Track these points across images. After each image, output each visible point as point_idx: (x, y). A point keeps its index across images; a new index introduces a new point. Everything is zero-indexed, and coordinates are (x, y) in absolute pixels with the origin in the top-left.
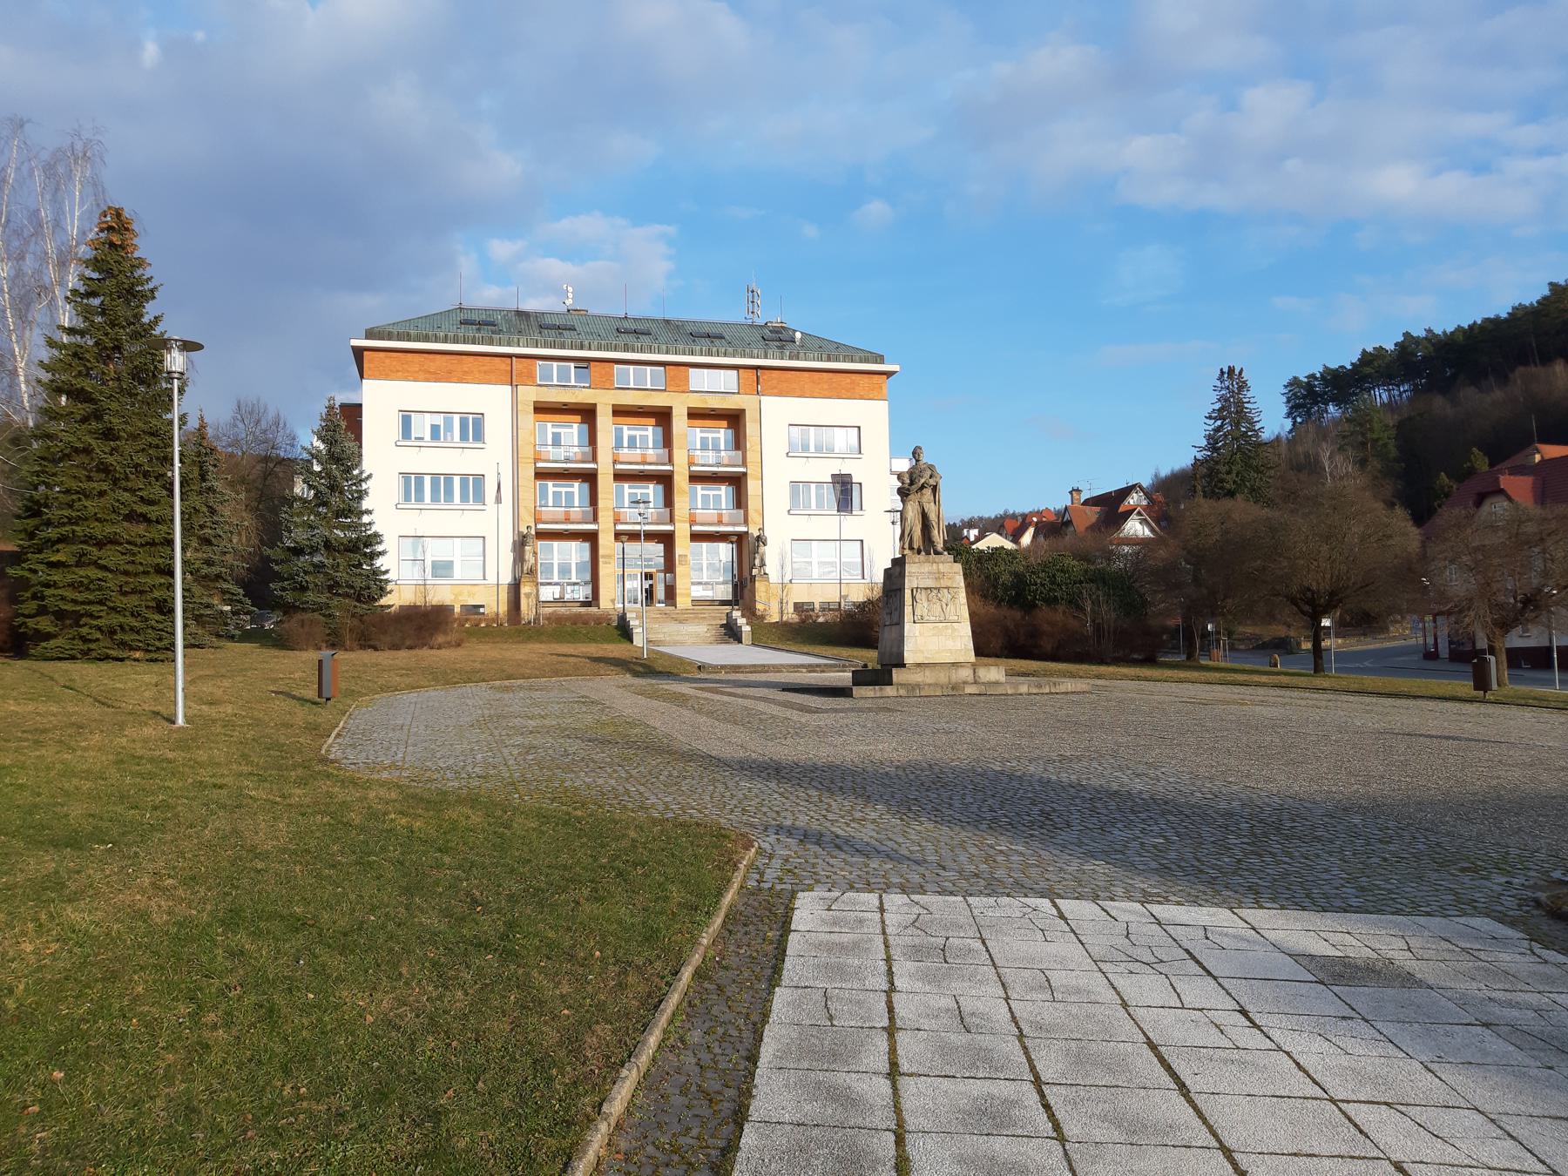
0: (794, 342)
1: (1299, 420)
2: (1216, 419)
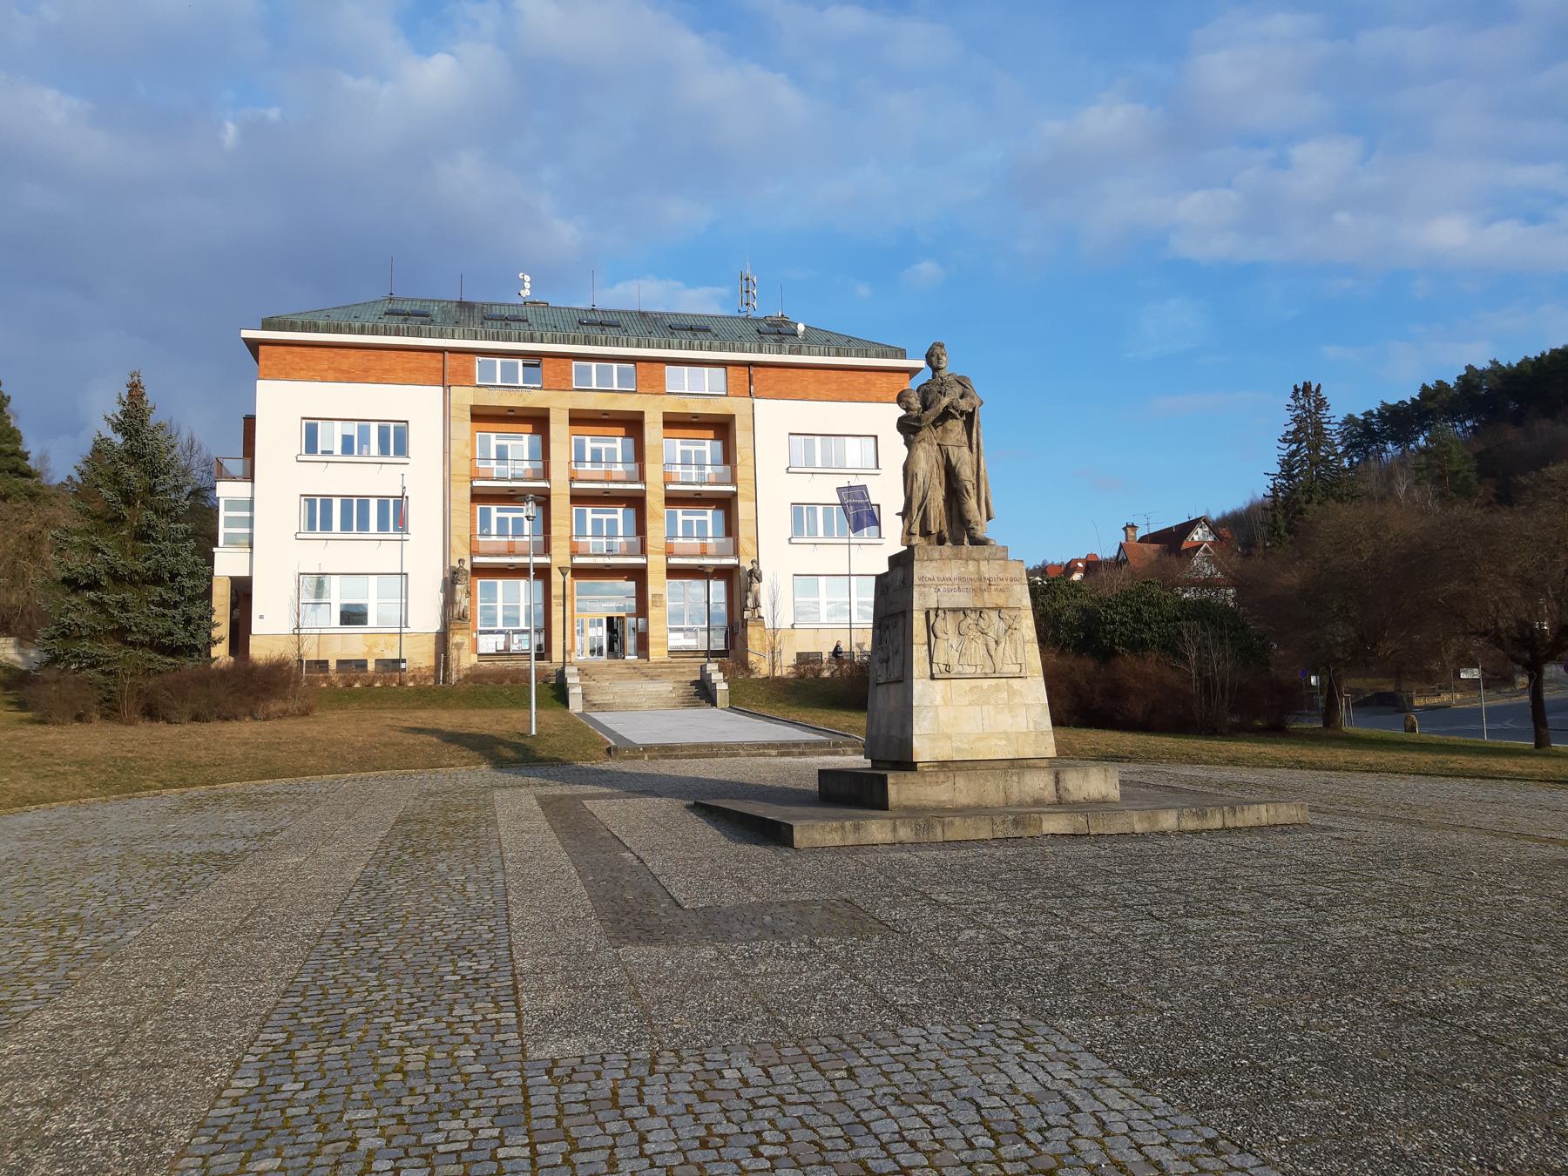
0: (796, 335)
1: (1356, 460)
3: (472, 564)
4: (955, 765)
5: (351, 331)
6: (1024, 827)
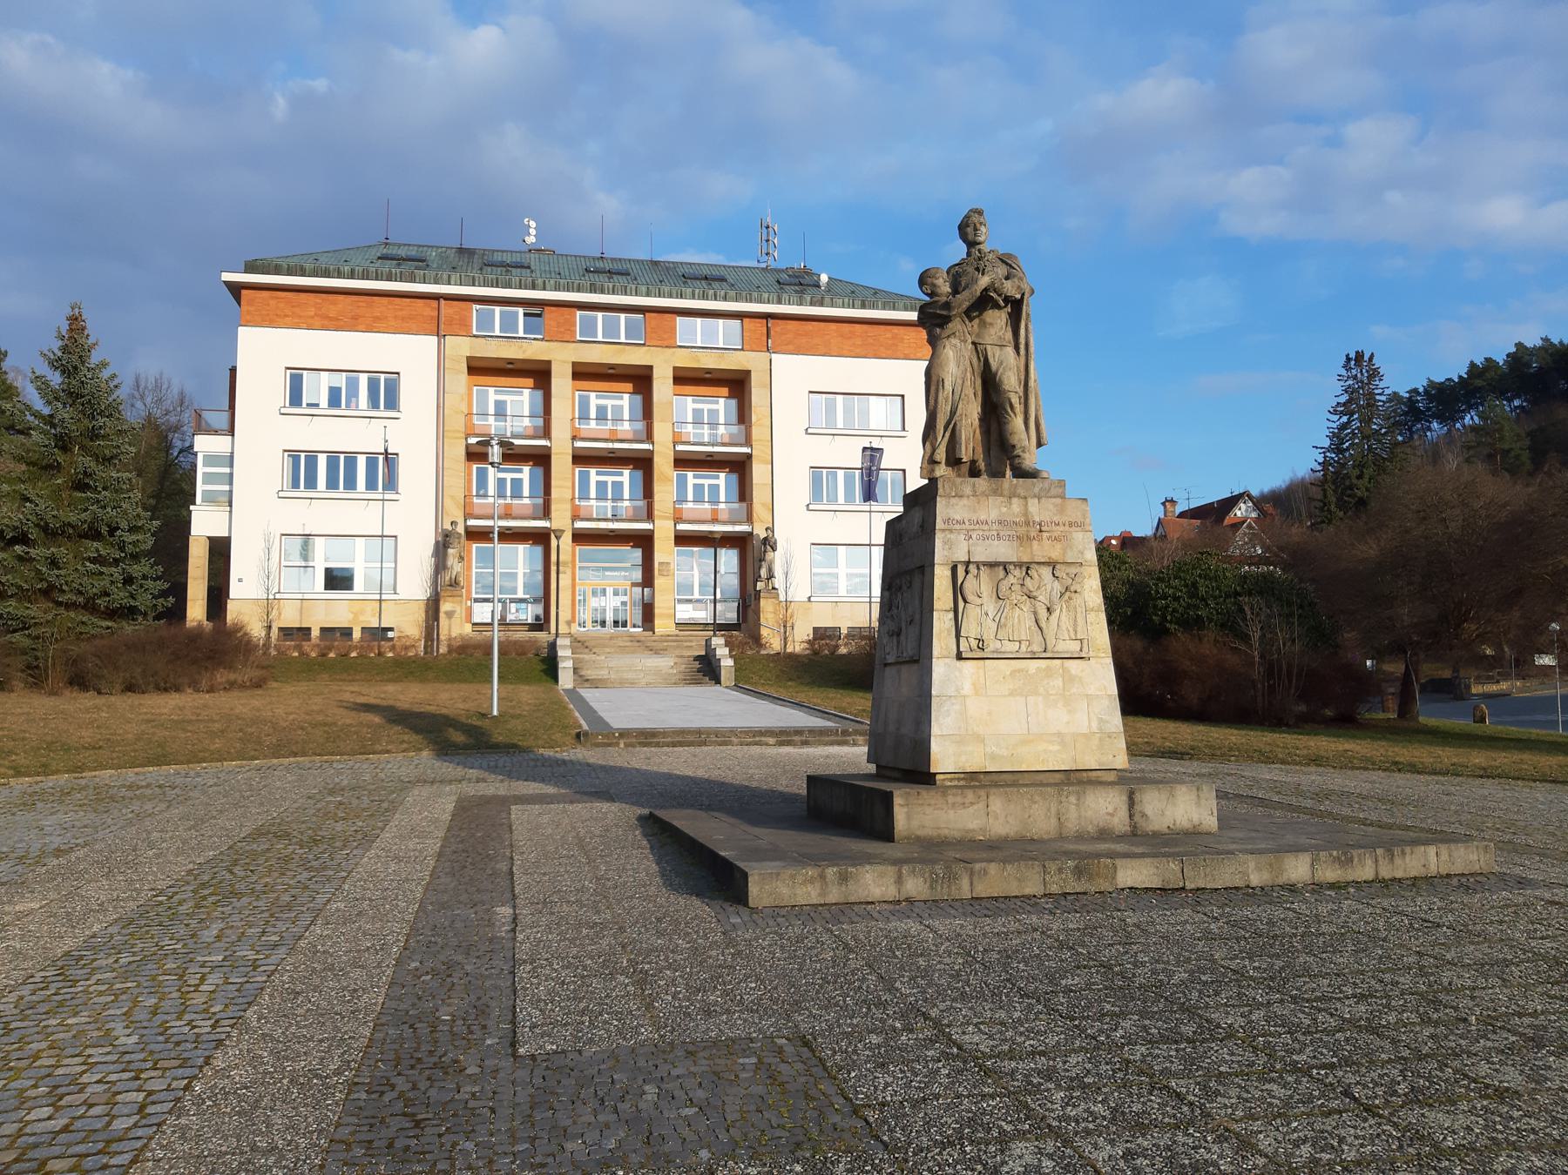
0: (819, 286)
3: (466, 528)
4: (989, 777)
5: (340, 275)
6: (1091, 878)
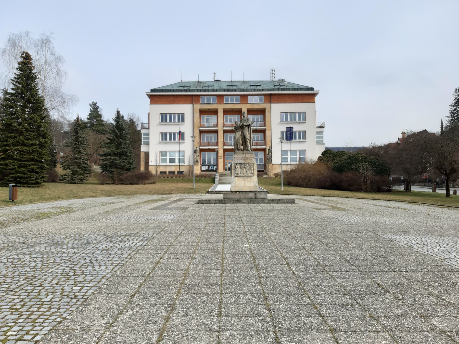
2: (453, 106)
3: (199, 149)
